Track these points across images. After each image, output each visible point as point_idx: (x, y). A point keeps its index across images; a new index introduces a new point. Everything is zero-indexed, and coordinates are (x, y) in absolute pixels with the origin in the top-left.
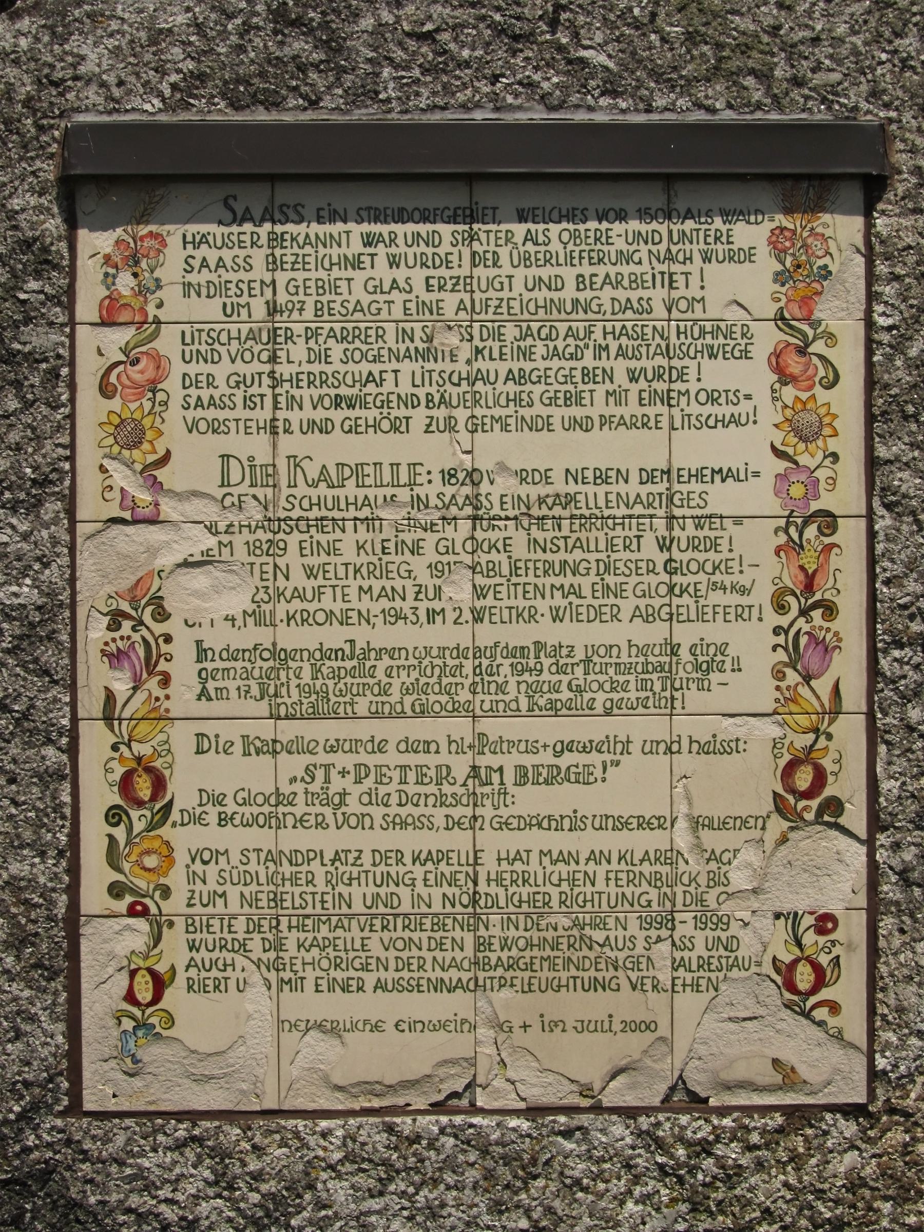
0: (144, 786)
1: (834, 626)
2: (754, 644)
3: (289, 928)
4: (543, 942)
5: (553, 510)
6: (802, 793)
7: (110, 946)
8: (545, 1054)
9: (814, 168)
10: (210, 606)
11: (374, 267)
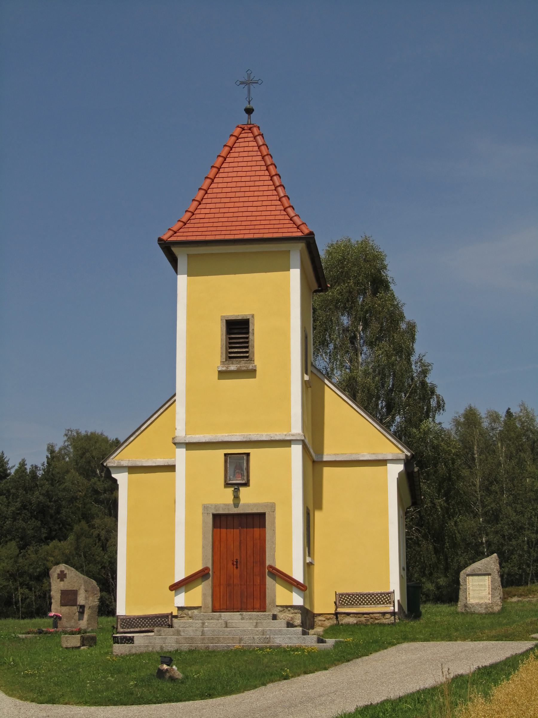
0: (469, 594)
1: (39, 465)
2: (487, 589)
3: (474, 598)
4: (481, 598)
5: (481, 585)
6: (489, 593)
7: (468, 599)
8: (482, 601)
9: (489, 574)
10: (471, 588)
11: (476, 578)
